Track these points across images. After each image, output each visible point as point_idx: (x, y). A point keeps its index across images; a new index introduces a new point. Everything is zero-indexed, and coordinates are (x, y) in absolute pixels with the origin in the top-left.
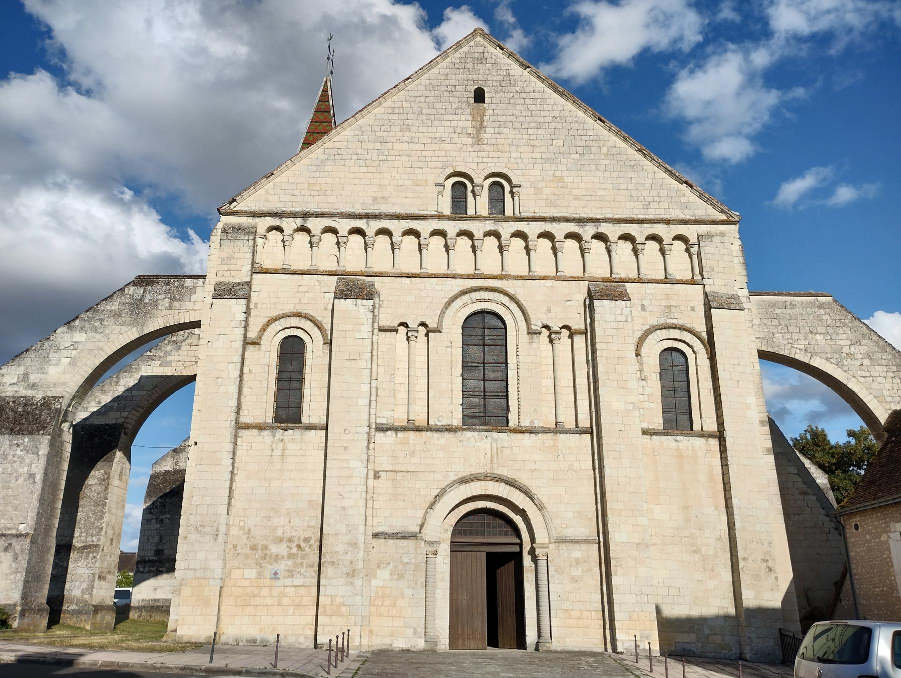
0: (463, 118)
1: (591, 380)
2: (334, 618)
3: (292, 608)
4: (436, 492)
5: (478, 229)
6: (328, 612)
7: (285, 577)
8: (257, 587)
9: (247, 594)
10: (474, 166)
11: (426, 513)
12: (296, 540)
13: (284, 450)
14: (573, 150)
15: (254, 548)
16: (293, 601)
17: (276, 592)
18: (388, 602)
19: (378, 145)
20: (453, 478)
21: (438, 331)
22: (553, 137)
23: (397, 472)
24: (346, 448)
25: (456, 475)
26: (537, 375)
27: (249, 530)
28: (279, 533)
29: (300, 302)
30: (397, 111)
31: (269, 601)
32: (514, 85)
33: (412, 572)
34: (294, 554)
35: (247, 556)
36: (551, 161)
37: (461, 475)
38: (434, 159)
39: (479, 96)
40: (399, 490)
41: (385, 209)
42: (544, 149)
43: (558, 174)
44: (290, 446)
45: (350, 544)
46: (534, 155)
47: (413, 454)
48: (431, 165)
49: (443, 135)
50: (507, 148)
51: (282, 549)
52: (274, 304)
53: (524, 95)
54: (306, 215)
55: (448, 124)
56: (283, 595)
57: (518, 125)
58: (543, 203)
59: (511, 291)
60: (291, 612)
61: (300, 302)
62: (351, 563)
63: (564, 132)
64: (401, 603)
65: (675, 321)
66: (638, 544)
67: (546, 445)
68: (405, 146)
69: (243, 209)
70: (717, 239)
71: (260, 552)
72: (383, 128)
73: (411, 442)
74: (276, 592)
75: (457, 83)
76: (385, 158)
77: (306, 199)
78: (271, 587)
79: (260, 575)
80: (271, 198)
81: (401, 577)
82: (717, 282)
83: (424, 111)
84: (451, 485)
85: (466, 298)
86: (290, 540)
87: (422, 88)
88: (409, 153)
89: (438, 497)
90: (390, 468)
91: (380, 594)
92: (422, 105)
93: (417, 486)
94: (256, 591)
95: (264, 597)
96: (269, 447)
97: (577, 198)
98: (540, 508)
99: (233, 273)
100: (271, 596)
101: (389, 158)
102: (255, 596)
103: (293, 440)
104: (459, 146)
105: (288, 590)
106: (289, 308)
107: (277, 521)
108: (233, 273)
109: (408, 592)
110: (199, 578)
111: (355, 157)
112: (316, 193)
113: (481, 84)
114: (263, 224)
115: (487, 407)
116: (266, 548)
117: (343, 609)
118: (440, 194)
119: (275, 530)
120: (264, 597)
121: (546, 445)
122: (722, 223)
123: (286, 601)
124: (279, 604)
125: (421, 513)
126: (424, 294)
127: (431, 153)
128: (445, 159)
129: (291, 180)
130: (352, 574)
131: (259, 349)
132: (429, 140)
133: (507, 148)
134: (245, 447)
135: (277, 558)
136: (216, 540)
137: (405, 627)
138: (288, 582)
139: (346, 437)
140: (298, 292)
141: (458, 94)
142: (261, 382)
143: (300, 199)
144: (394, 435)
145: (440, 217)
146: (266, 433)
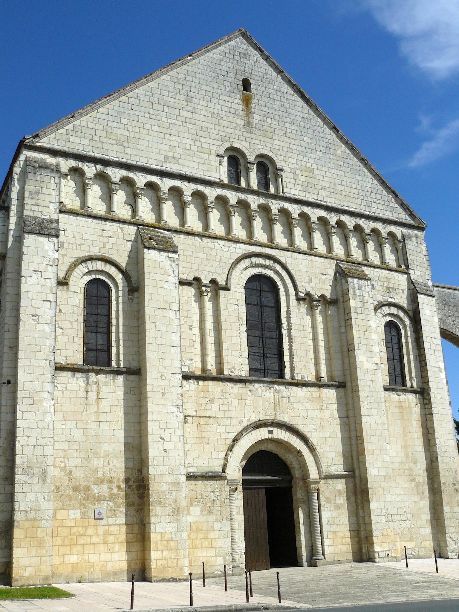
0: (235, 101)
1: (404, 344)
2: (165, 553)
3: (117, 545)
4: (233, 436)
5: (254, 201)
6: (160, 547)
7: (108, 517)
8: (82, 526)
9: (74, 534)
10: (246, 144)
11: (227, 455)
12: (115, 480)
13: (98, 392)
14: (318, 148)
15: (76, 489)
16: (118, 539)
17: (101, 530)
18: (201, 536)
19: (166, 109)
20: (245, 423)
21: (227, 289)
22: (303, 134)
23: (201, 417)
24: (163, 394)
25: (248, 421)
26: (303, 336)
27: (70, 471)
28: (100, 474)
29: (104, 247)
30: (181, 82)
31: (95, 540)
32: (272, 84)
33: (218, 508)
34: (115, 495)
35: (70, 498)
36: (305, 154)
37: (252, 421)
38: (214, 132)
39: (246, 85)
40: (204, 434)
41: (175, 169)
42: (297, 142)
43: (309, 165)
44: (104, 388)
45: (173, 484)
46: (291, 146)
47: (211, 401)
48: (213, 136)
49: (220, 112)
50: (270, 135)
51: (104, 490)
52: (80, 245)
53: (279, 93)
54: (106, 163)
55: (223, 103)
56: (107, 533)
57: (277, 118)
58: (300, 188)
59: (283, 260)
60: (116, 549)
61: (104, 247)
62: (176, 501)
63: (310, 131)
64: (212, 535)
65: (392, 300)
66: (384, 476)
67: (314, 396)
68: (189, 115)
69: (45, 145)
70: (414, 239)
71: (82, 494)
72: (170, 94)
73: (210, 390)
74: (101, 530)
75: (228, 70)
76: (173, 121)
77: (105, 146)
78: (96, 526)
79: (84, 516)
80: (72, 139)
81: (210, 513)
82: (418, 273)
83: (204, 87)
84: (245, 429)
85: (247, 262)
86: (110, 481)
87: (200, 66)
88: (193, 121)
89: (235, 440)
90: (194, 414)
91: (194, 529)
92: (202, 81)
93: (218, 431)
94: (82, 531)
95: (90, 536)
96: (83, 389)
97: (323, 188)
98: (312, 449)
99: (41, 209)
100: (97, 534)
101: (177, 123)
102: (81, 536)
103: (106, 383)
104: (234, 125)
105: (112, 528)
106: (94, 251)
107: (97, 462)
108: (41, 209)
109: (217, 526)
110: (31, 520)
111: (147, 115)
112: (114, 142)
113: (247, 76)
114: (66, 164)
115: (268, 360)
116: (88, 488)
117: (172, 544)
118: (221, 163)
119: (96, 471)
120: (90, 536)
121: (314, 396)
122: (411, 227)
123: (111, 539)
124: (105, 542)
125: (223, 455)
126: (214, 253)
127: (211, 126)
128: (223, 134)
129: (91, 125)
130: (177, 511)
131: (68, 289)
132: (210, 115)
133: (270, 135)
134: (60, 388)
135: (99, 499)
136: (44, 481)
137: (216, 556)
138: (111, 521)
139: (163, 383)
140: (102, 236)
141: (230, 80)
142: (71, 322)
143: (99, 145)
144: (196, 383)
145: (222, 185)
146: (79, 375)
